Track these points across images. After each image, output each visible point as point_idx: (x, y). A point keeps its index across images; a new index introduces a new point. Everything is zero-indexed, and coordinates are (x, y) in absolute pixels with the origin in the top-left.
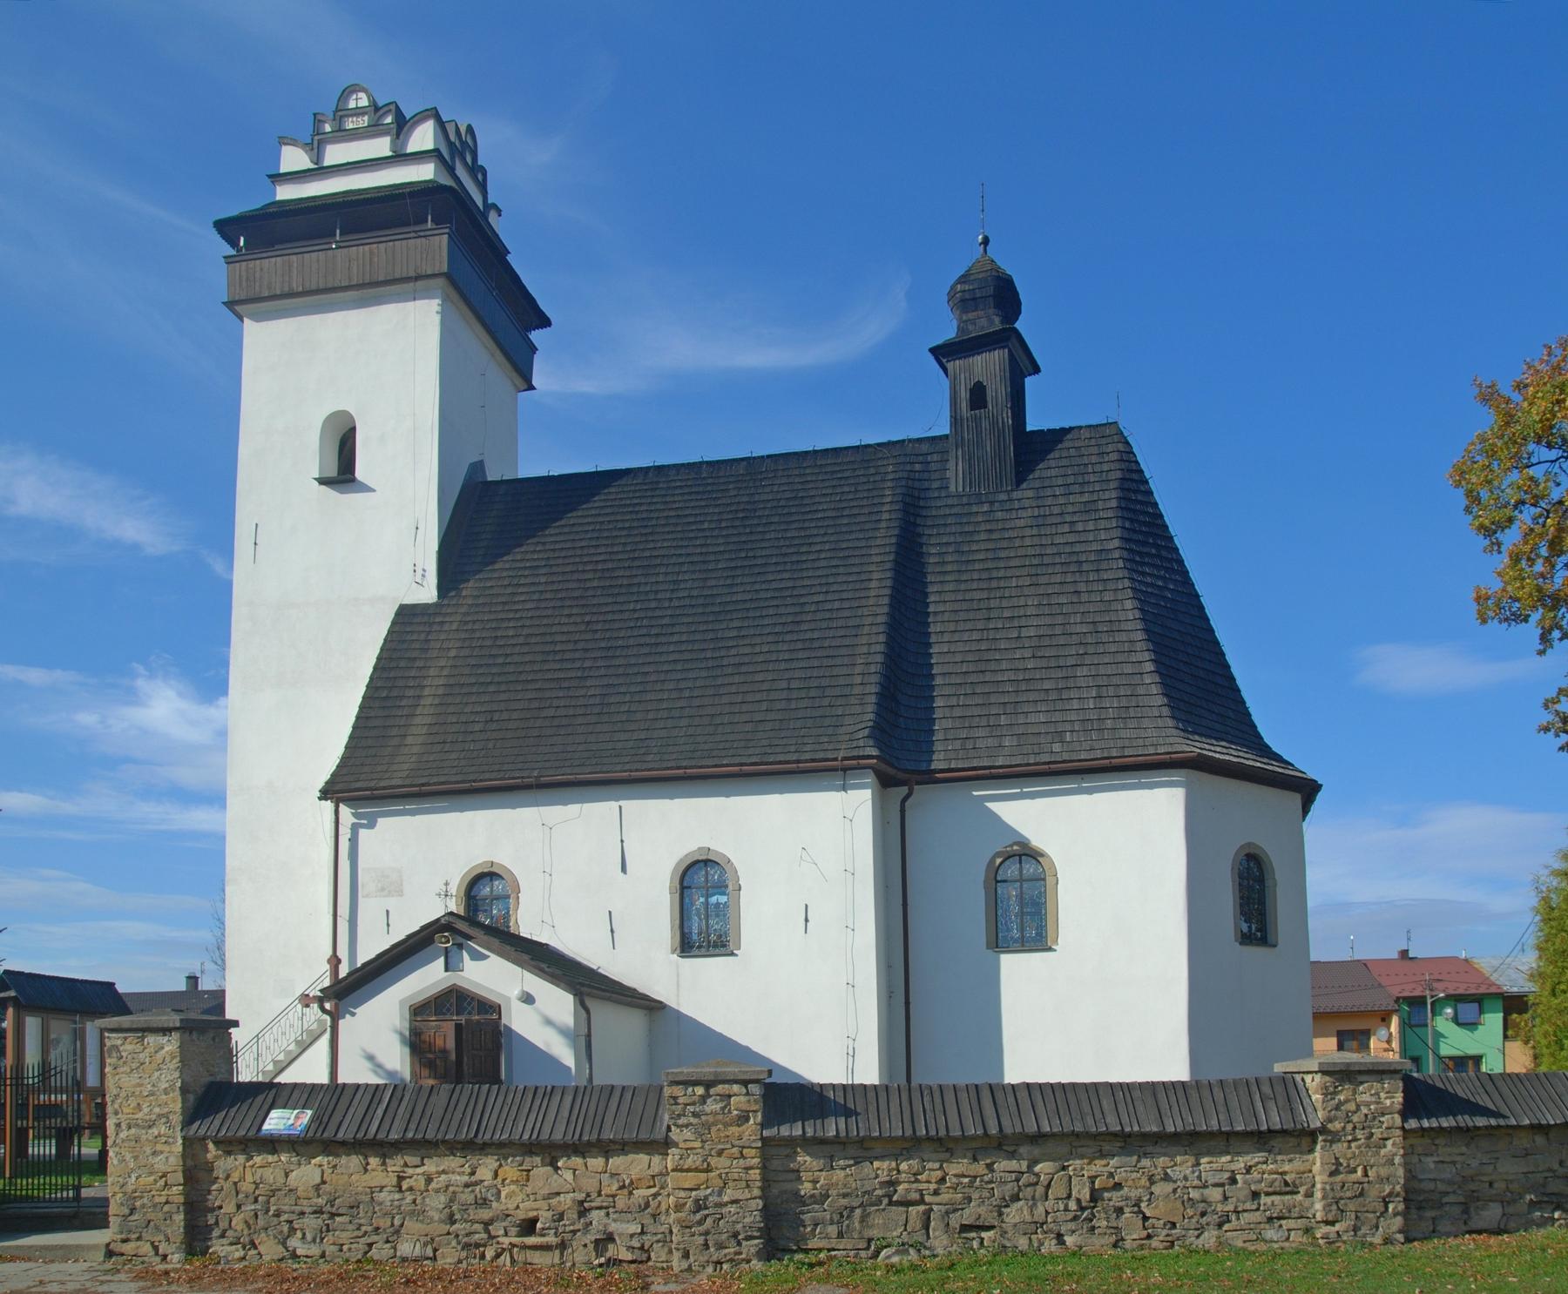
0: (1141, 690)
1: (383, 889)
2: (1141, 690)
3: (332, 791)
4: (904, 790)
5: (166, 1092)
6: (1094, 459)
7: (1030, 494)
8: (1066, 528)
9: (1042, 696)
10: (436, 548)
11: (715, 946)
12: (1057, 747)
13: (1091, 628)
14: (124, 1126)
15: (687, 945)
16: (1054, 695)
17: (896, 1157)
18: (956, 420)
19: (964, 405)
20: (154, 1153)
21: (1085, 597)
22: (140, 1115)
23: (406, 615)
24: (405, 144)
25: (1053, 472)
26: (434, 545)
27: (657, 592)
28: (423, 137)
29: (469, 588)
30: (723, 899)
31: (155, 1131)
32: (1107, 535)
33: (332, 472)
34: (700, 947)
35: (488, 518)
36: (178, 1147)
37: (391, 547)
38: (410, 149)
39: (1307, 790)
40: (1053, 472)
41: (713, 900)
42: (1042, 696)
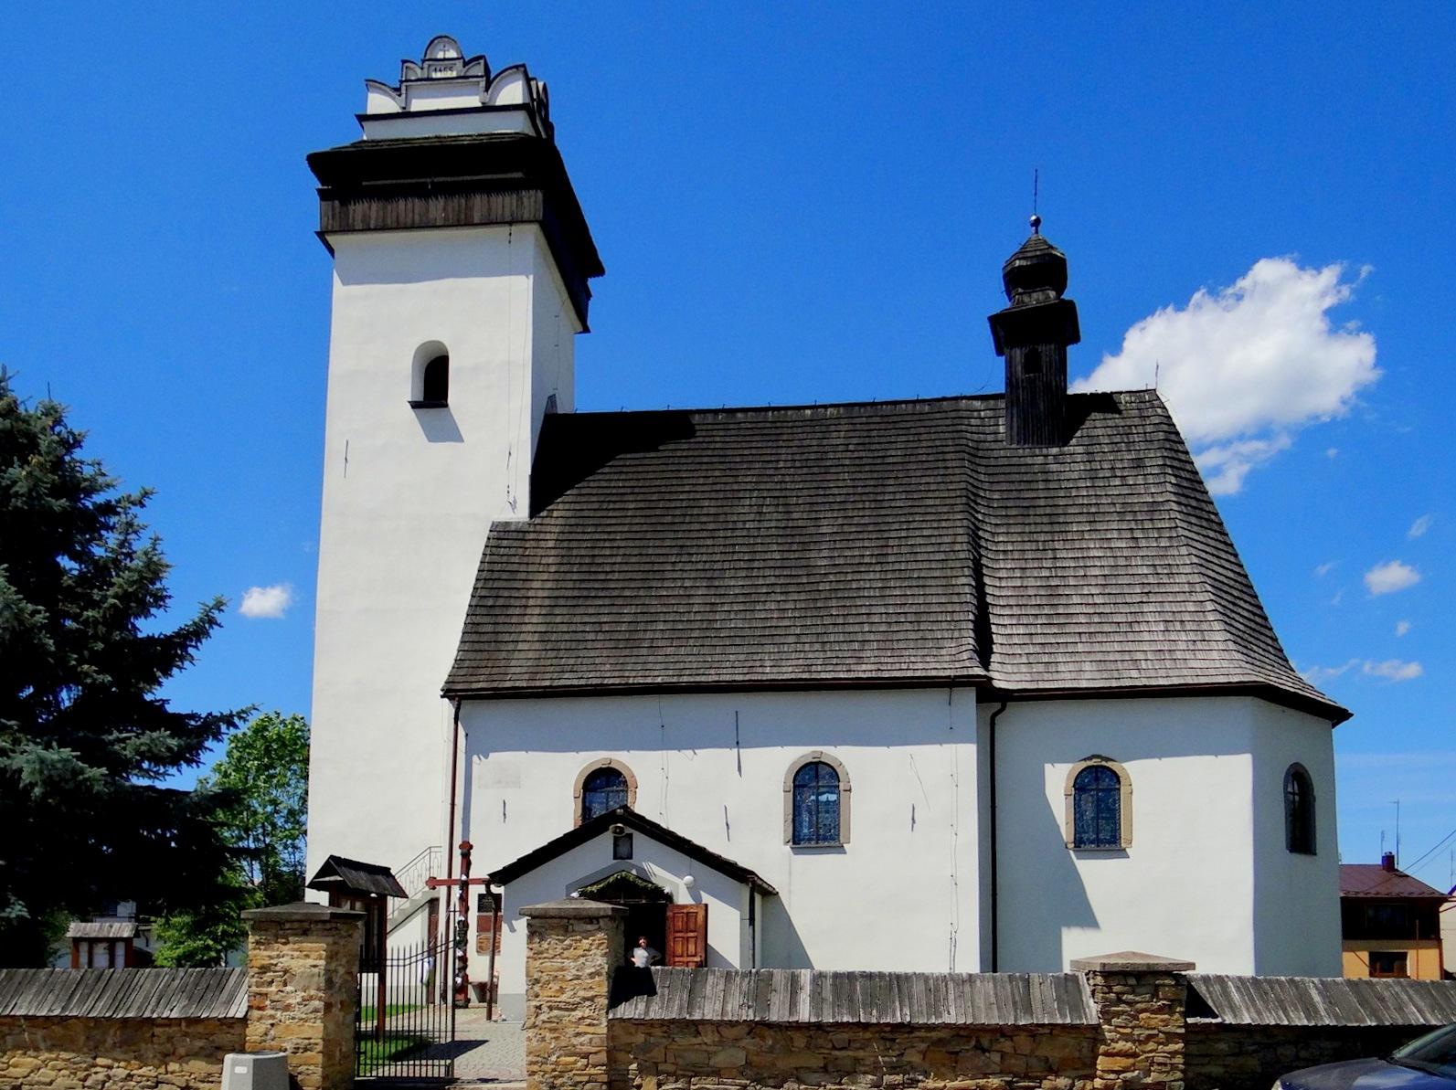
0: (1205, 626)
1: (500, 782)
2: (1205, 626)
3: (448, 693)
4: (997, 706)
5: (592, 975)
6: (1137, 421)
7: (1080, 450)
8: (1117, 482)
9: (1114, 628)
10: (529, 471)
11: (825, 839)
12: (1134, 674)
13: (1151, 570)
14: (545, 1008)
15: (798, 840)
16: (1124, 628)
17: (723, 1021)
18: (1010, 382)
19: (1019, 368)
20: (578, 1034)
21: (1143, 543)
22: (564, 998)
23: (502, 535)
24: (494, 97)
25: (1100, 432)
26: (527, 470)
27: (744, 522)
28: (512, 92)
29: (560, 510)
30: (833, 797)
31: (578, 1014)
32: (1164, 491)
33: (420, 398)
34: (810, 840)
35: (571, 449)
36: (603, 1029)
37: (492, 465)
38: (500, 102)
39: (1338, 715)
40: (1100, 432)
41: (823, 798)
42: (1114, 628)
